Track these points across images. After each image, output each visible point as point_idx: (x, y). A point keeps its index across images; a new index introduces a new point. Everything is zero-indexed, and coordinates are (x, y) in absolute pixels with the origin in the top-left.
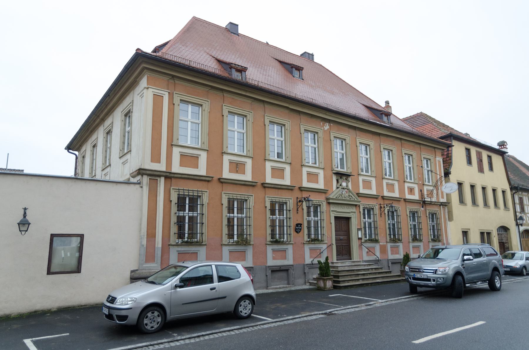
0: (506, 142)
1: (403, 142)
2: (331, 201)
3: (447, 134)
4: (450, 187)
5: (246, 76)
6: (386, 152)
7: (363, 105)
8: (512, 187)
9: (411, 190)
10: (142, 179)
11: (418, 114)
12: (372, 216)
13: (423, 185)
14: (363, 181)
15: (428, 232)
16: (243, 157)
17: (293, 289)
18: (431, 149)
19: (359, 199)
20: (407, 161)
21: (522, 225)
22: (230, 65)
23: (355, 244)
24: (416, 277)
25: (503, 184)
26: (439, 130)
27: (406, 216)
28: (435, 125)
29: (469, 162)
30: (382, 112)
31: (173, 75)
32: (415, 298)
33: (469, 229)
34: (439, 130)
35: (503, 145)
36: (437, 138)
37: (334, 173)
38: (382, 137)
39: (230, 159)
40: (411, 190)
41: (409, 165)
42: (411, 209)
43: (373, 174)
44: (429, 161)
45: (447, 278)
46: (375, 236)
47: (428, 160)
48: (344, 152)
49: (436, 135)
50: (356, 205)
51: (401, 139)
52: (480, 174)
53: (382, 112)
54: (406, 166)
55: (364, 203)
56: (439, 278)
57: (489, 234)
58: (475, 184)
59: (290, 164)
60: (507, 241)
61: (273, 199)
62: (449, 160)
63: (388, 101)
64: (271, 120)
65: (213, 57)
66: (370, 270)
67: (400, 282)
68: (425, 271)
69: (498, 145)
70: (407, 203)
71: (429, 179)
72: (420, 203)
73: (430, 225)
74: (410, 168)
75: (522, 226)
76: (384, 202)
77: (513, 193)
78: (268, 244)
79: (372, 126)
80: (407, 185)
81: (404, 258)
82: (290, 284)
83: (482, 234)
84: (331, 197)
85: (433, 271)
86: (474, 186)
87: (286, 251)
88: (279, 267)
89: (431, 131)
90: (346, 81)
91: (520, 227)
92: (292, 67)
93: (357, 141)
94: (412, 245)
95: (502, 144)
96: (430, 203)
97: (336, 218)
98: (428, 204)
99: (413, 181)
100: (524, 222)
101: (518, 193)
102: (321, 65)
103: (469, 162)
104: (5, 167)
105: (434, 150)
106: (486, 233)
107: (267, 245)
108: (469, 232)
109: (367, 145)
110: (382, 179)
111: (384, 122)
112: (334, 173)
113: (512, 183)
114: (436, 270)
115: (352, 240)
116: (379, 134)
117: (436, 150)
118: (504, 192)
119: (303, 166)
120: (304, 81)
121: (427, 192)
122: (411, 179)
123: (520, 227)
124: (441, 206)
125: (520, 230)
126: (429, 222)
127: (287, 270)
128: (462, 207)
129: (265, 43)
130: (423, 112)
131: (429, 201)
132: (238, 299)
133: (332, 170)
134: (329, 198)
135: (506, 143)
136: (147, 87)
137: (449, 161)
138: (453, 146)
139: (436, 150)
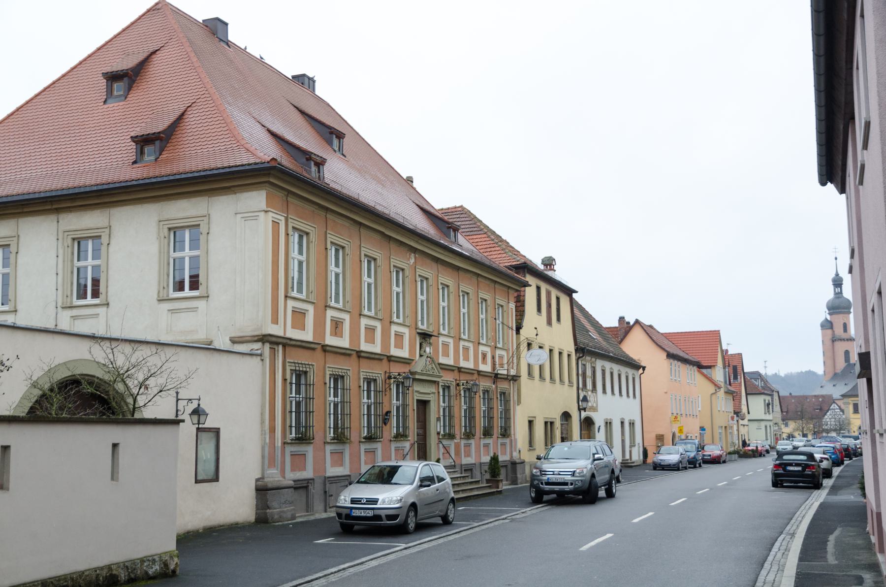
0: (554, 260)
1: (480, 279)
2: (417, 377)
3: (520, 264)
4: (538, 356)
5: (324, 175)
6: (296, 236)
7: (417, 205)
8: (577, 348)
9: (299, 316)
10: (263, 348)
11: (456, 208)
12: (303, 388)
13: (496, 347)
14: (365, 328)
15: (325, 421)
16: (343, 312)
17: (312, 518)
18: (504, 289)
19: (442, 373)
20: (296, 246)
21: (585, 409)
23: (433, 440)
24: (551, 481)
25: (569, 346)
26: (503, 252)
27: (323, 384)
28: (493, 240)
30: (450, 225)
31: (289, 190)
32: (546, 508)
33: (535, 417)
34: (503, 252)
35: (551, 265)
36: (505, 266)
37: (419, 333)
38: (461, 273)
40: (337, 325)
41: (300, 258)
42: (446, 382)
43: (310, 298)
44: (500, 308)
45: (585, 480)
47: (371, 259)
48: (425, 299)
49: (502, 262)
50: (434, 382)
51: (478, 275)
52: (548, 327)
53: (450, 225)
54: (365, 282)
55: (448, 378)
56: (577, 480)
57: (552, 423)
59: (380, 321)
61: (368, 374)
62: (520, 306)
63: (411, 177)
64: (333, 240)
65: (263, 126)
66: (459, 479)
67: (494, 495)
68: (561, 473)
69: (542, 264)
70: (330, 357)
71: (337, 294)
72: (491, 377)
73: (291, 402)
74: (300, 263)
76: (359, 362)
78: (362, 442)
79: (457, 258)
80: (330, 313)
81: (491, 461)
82: (308, 512)
83: (546, 423)
84: (418, 370)
85: (570, 473)
87: (374, 451)
88: (306, 482)
89: (489, 250)
91: (582, 412)
92: (331, 133)
93: (289, 223)
94: (330, 449)
95: (549, 262)
96: (506, 377)
98: (503, 378)
99: (340, 306)
100: (590, 404)
101: (584, 358)
102: (328, 105)
103: (539, 309)
105: (507, 290)
106: (549, 423)
107: (361, 444)
108: (534, 421)
109: (424, 277)
110: (458, 339)
112: (419, 333)
114: (574, 472)
115: (430, 435)
116: (458, 269)
117: (509, 291)
118: (569, 355)
119: (392, 324)
120: (346, 159)
121: (395, 336)
122: (337, 301)
123: (582, 412)
124: (512, 382)
126: (288, 395)
127: (471, 470)
129: (198, 22)
130: (465, 206)
131: (504, 375)
133: (416, 329)
134: (416, 372)
135: (554, 261)
136: (266, 209)
137: (521, 307)
139: (509, 291)
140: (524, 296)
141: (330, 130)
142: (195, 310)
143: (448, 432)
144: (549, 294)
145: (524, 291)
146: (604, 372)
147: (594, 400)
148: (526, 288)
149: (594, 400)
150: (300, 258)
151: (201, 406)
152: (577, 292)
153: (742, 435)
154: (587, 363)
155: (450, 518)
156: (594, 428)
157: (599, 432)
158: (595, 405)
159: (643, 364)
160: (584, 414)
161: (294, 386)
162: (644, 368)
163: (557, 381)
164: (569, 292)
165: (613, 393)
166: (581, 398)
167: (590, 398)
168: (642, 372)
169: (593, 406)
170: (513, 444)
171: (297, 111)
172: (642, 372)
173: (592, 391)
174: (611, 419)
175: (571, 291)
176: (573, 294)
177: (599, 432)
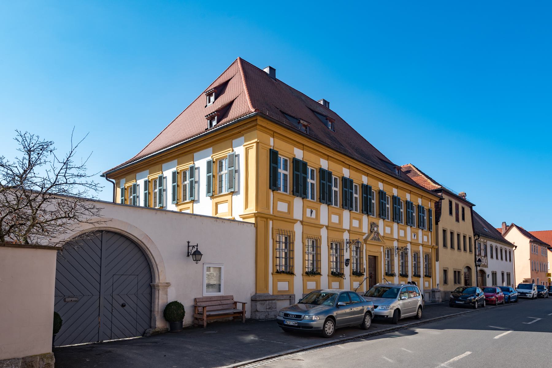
21: (479, 266)
22: (298, 120)
24: (286, 324)
25: (470, 232)
29: (451, 213)
39: (279, 198)
41: (285, 172)
46: (391, 272)
48: (389, 206)
57: (459, 272)
58: (453, 231)
60: (468, 279)
75: (479, 267)
77: (475, 239)
83: (455, 272)
86: (453, 233)
90: (355, 129)
97: (369, 255)
103: (451, 213)
104: (192, 213)
111: (396, 175)
113: (476, 230)
118: (470, 238)
125: (478, 270)
128: (444, 250)
132: (323, 325)
138: (444, 199)
140: (441, 205)
141: (326, 118)
142: (226, 202)
143: (288, 270)
144: (457, 206)
145: (441, 202)
146: (492, 247)
147: (486, 262)
148: (442, 200)
149: (486, 262)
150: (285, 172)
151: (198, 250)
152: (475, 205)
153: (470, 251)
154: (482, 243)
155: (366, 325)
156: (486, 276)
157: (488, 278)
158: (486, 264)
159: (515, 245)
160: (479, 268)
161: (386, 255)
162: (516, 247)
163: (448, 247)
164: (471, 205)
165: (497, 258)
166: (477, 260)
167: (483, 260)
168: (515, 249)
169: (485, 264)
170: (434, 281)
171: (309, 110)
172: (515, 249)
173: (484, 257)
174: (509, 272)
175: (472, 205)
176: (473, 207)
177: (488, 278)
